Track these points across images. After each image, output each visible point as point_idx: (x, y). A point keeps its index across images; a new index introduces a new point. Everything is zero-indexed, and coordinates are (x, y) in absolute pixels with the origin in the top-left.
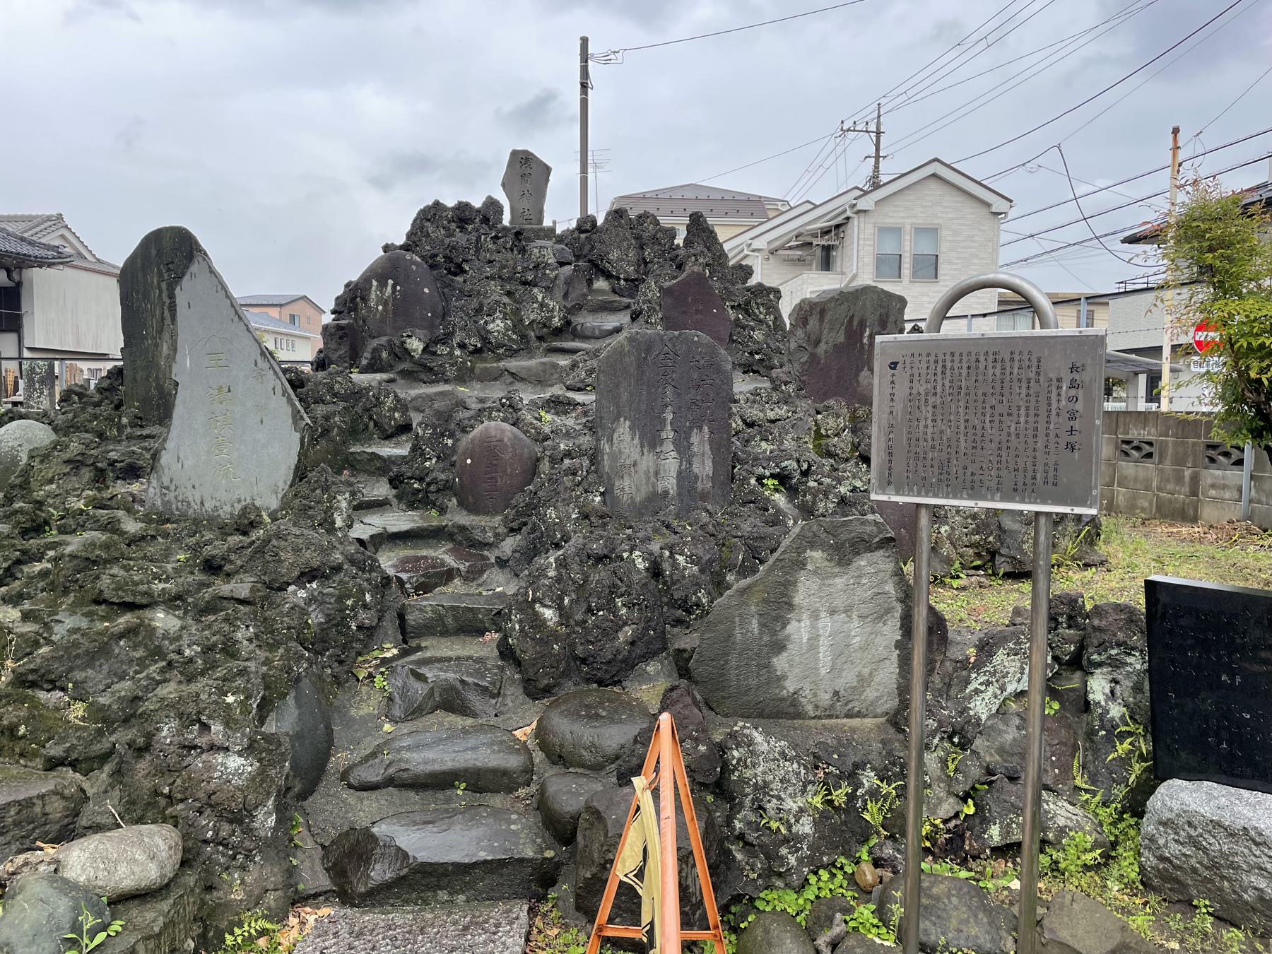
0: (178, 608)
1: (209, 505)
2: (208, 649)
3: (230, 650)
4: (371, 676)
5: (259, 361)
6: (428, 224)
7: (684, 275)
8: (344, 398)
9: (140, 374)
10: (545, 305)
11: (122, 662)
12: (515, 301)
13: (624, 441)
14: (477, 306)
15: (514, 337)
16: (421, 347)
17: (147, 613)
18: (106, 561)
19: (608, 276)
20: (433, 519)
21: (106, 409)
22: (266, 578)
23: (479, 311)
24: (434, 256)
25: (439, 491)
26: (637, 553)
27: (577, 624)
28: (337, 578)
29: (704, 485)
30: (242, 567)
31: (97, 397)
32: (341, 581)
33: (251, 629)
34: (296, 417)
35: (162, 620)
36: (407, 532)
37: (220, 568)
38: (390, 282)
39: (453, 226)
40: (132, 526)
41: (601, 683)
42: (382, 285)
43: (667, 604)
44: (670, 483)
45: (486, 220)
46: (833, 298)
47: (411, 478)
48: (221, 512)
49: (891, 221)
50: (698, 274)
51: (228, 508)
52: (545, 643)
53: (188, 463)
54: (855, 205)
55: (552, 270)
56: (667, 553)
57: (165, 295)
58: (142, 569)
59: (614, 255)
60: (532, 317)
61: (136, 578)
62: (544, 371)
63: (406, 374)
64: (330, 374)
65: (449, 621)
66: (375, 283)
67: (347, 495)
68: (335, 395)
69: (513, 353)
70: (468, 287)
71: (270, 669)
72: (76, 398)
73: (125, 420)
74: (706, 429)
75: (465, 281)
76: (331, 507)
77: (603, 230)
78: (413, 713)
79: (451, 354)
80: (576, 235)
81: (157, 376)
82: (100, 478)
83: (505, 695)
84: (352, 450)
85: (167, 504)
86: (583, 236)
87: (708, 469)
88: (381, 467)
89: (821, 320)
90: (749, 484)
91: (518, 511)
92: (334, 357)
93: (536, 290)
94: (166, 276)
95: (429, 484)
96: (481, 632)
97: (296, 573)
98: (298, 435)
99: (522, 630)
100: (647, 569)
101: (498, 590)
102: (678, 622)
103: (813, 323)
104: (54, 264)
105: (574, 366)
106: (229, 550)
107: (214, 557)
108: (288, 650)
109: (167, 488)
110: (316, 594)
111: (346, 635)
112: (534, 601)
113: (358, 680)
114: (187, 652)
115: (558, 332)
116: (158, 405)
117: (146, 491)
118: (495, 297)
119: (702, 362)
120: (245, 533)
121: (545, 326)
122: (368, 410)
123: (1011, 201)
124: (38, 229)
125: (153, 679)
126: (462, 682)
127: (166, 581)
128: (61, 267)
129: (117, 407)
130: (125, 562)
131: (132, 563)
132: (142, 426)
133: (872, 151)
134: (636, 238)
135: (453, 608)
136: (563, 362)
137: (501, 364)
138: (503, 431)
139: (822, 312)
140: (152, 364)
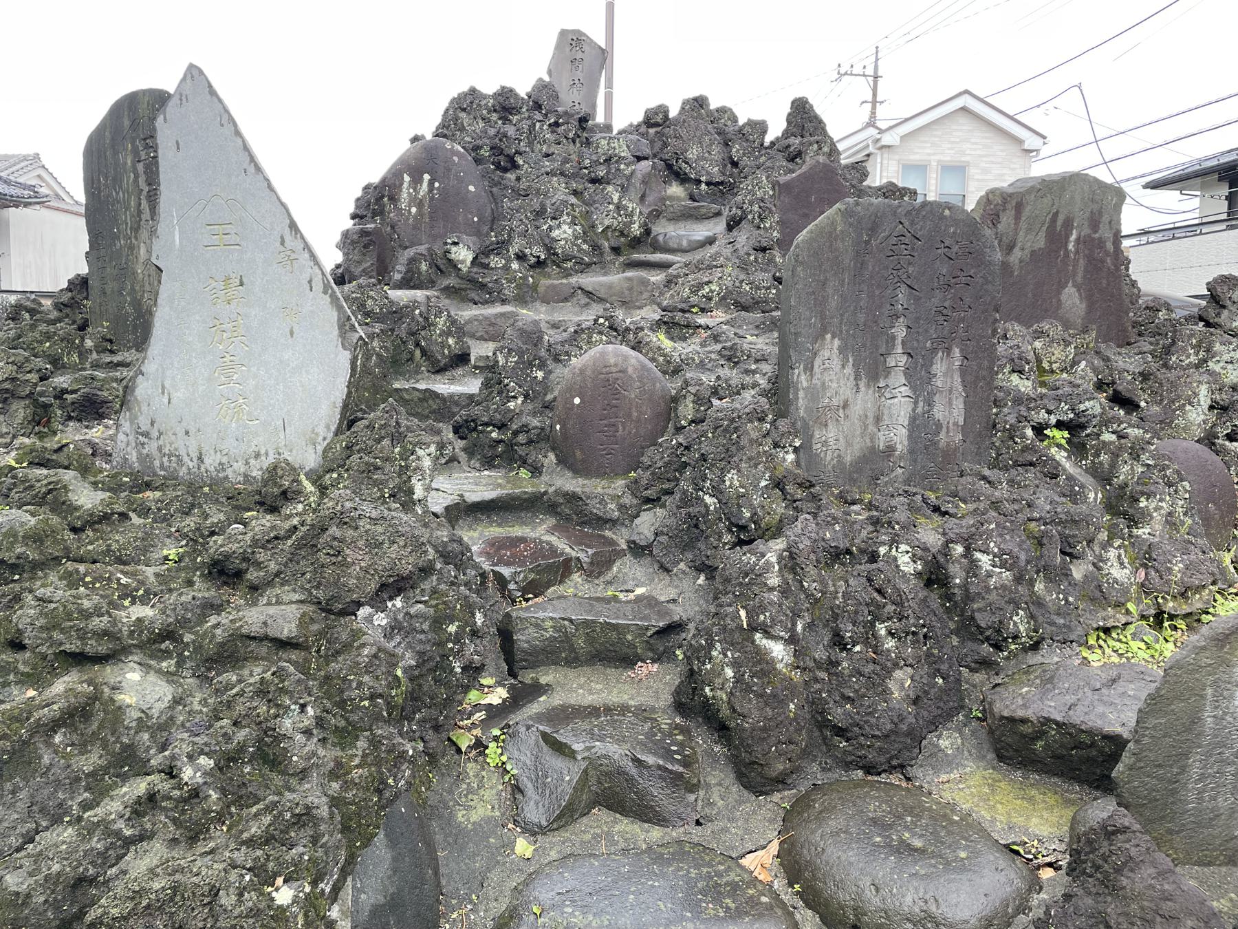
0: (166, 654)
1: (211, 462)
2: (228, 761)
3: (270, 753)
4: (480, 746)
5: (288, 238)
6: (463, 115)
7: (804, 168)
8: (380, 319)
9: (111, 286)
10: (621, 207)
11: (58, 783)
12: (585, 203)
13: (829, 373)
14: (537, 207)
15: (585, 247)
16: (470, 257)
17: (109, 673)
18: (36, 566)
19: (682, 178)
20: (523, 483)
21: (64, 328)
22: (320, 594)
23: (540, 213)
24: (476, 148)
25: (530, 442)
26: (903, 547)
27: (819, 665)
28: (426, 585)
29: (951, 437)
30: (277, 575)
31: (54, 314)
32: (434, 591)
33: (310, 711)
34: (345, 327)
35: (139, 688)
36: (492, 501)
37: (239, 574)
38: (427, 177)
39: (494, 116)
40: (86, 498)
41: (869, 769)
42: (416, 181)
43: (956, 632)
44: (898, 435)
45: (538, 106)
46: (1033, 187)
47: (487, 424)
48: (229, 472)
49: (917, 157)
50: (825, 165)
51: (239, 467)
52: (778, 701)
53: (178, 396)
54: (878, 140)
55: (627, 165)
56: (959, 549)
57: (142, 180)
58: (99, 579)
59: (693, 153)
60: (607, 222)
61: (86, 604)
62: (631, 289)
63: (449, 291)
64: (360, 286)
65: (580, 642)
66: (407, 178)
67: (433, 449)
68: (367, 314)
69: (584, 267)
70: (523, 185)
71: (346, 786)
72: (27, 316)
73: (89, 343)
74: (956, 352)
75: (518, 179)
76: (407, 467)
77: (676, 122)
78: (559, 817)
79: (506, 268)
80: (643, 129)
81: (133, 289)
82: (41, 418)
83: (708, 786)
84: (397, 385)
85: (145, 459)
86: (652, 131)
87: (957, 412)
88: (440, 408)
89: (1017, 217)
90: (1023, 436)
91: (653, 473)
92: (358, 271)
93: (610, 188)
94: (143, 155)
95: (516, 433)
96: (628, 661)
97: (373, 586)
98: (347, 355)
99: (738, 679)
100: (918, 575)
101: (640, 591)
102: (985, 664)
103: (1006, 219)
104: (30, 204)
105: (669, 282)
106: (255, 543)
107: (227, 556)
108: (375, 743)
109: (146, 434)
110: (400, 617)
111: (447, 685)
112: (753, 628)
113: (459, 751)
114: (187, 774)
115: (636, 243)
116: (135, 327)
117: (112, 438)
118: (560, 196)
119: (955, 248)
120: (273, 510)
121: (622, 234)
122: (413, 334)
123: (1044, 137)
124: (14, 169)
125: (118, 834)
126: (636, 760)
127: (144, 601)
128: (38, 207)
129: (82, 328)
130: (70, 566)
131: (82, 568)
132: (112, 352)
133: (870, 98)
134: (719, 134)
135: (586, 623)
136: (657, 277)
137: (574, 280)
138: (626, 358)
139: (1019, 207)
140: (125, 272)
